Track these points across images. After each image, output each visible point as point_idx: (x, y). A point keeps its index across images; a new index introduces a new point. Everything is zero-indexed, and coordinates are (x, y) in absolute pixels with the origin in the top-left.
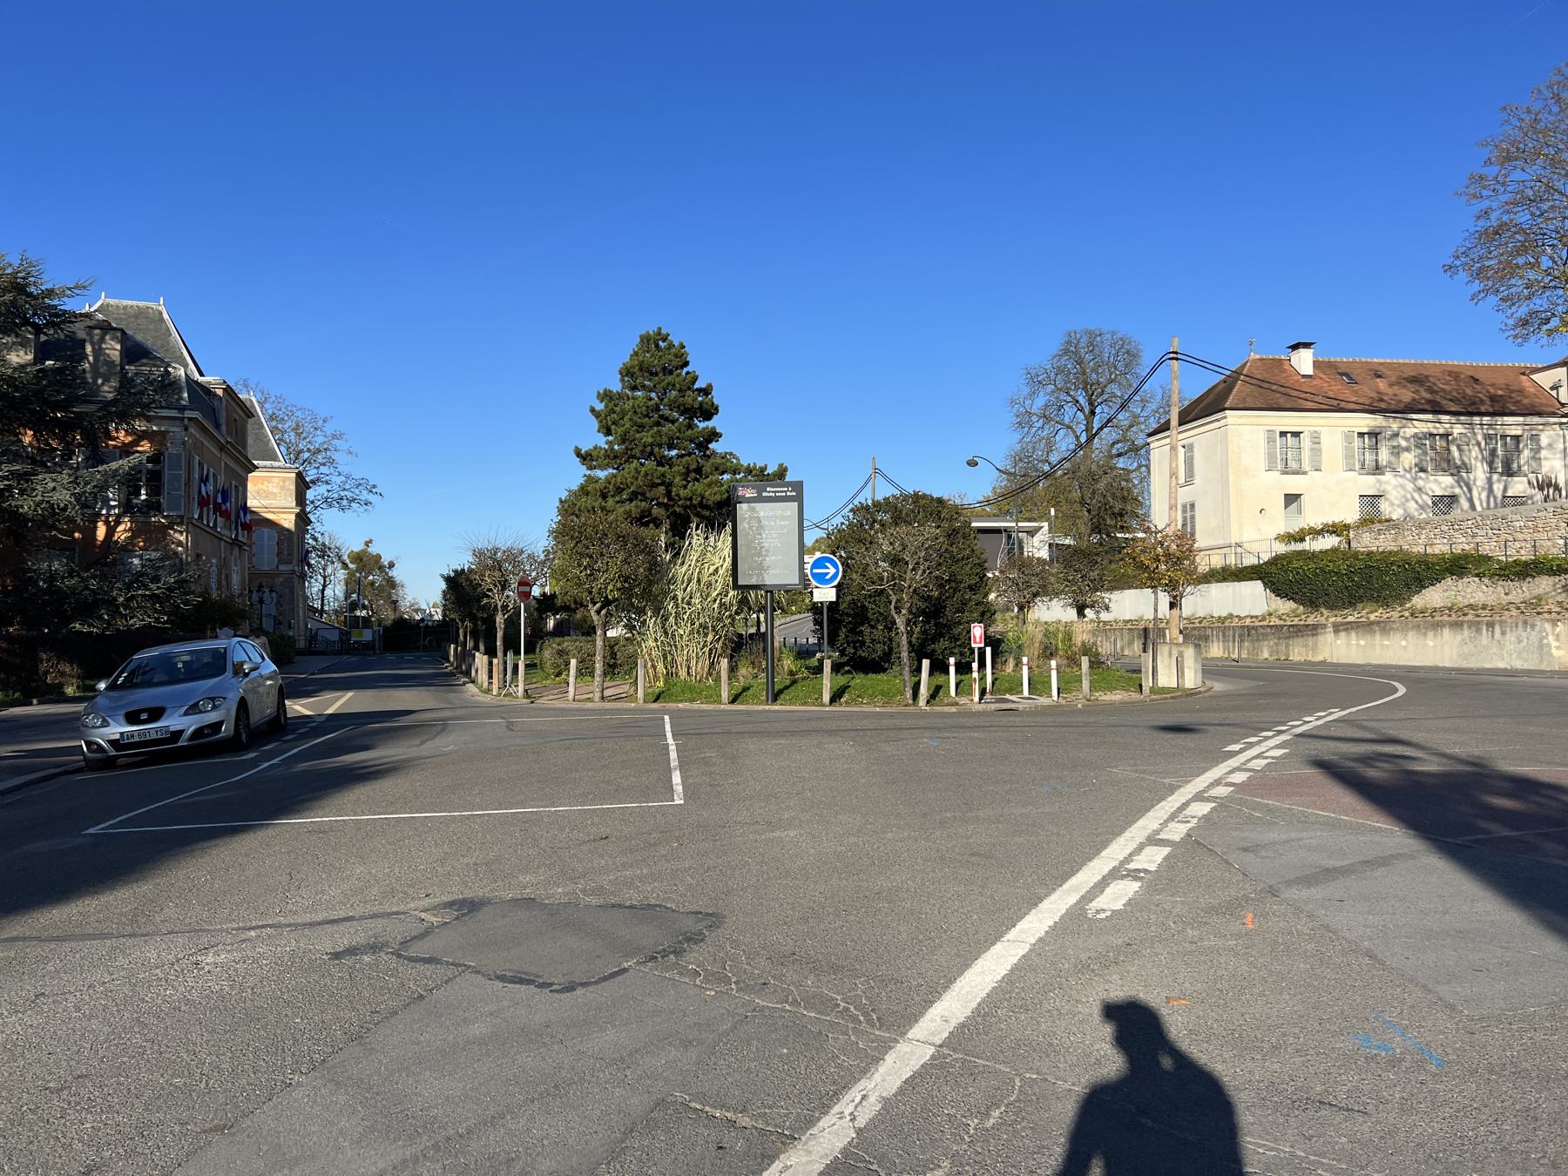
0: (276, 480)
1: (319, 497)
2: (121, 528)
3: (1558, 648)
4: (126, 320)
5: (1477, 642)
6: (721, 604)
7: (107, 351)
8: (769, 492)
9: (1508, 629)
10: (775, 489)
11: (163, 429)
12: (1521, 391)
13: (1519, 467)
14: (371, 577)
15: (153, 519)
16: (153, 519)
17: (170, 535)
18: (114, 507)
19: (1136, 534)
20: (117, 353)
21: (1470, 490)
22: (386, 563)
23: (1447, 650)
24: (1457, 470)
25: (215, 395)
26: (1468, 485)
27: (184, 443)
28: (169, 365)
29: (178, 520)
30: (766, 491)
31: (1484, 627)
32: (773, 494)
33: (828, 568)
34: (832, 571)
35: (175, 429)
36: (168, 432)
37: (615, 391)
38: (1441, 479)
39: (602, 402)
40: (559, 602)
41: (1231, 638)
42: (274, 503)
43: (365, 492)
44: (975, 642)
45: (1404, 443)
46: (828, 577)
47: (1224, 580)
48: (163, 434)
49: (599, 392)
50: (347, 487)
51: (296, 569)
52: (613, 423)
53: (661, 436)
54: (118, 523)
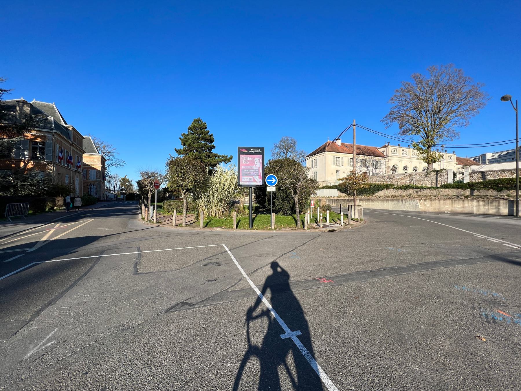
0: (96, 158)
1: (110, 164)
2: (29, 164)
3: (421, 206)
4: (41, 107)
5: (398, 204)
6: (228, 191)
7: (25, 110)
8: (252, 151)
9: (407, 201)
10: (254, 150)
11: (45, 135)
12: (377, 152)
13: (377, 167)
14: (126, 184)
15: (41, 162)
16: (41, 162)
17: (47, 167)
18: (27, 158)
19: (123, 191)
20: (29, 111)
21: (369, 171)
22: (130, 181)
23: (390, 206)
24: (368, 167)
25: (69, 130)
26: (369, 170)
27: (52, 140)
28: (48, 116)
29: (50, 163)
30: (251, 151)
31: (400, 201)
32: (254, 152)
33: (273, 179)
34: (274, 180)
35: (50, 136)
36: (47, 136)
37: (186, 134)
38: (364, 169)
39: (183, 136)
40: (169, 190)
41: (332, 202)
42: (95, 164)
43: (122, 163)
44: (312, 206)
45: (358, 161)
46: (273, 183)
47: (327, 188)
48: (45, 137)
49: (182, 134)
50: (117, 161)
51: (102, 180)
52: (186, 141)
53: (199, 145)
54: (28, 162)
